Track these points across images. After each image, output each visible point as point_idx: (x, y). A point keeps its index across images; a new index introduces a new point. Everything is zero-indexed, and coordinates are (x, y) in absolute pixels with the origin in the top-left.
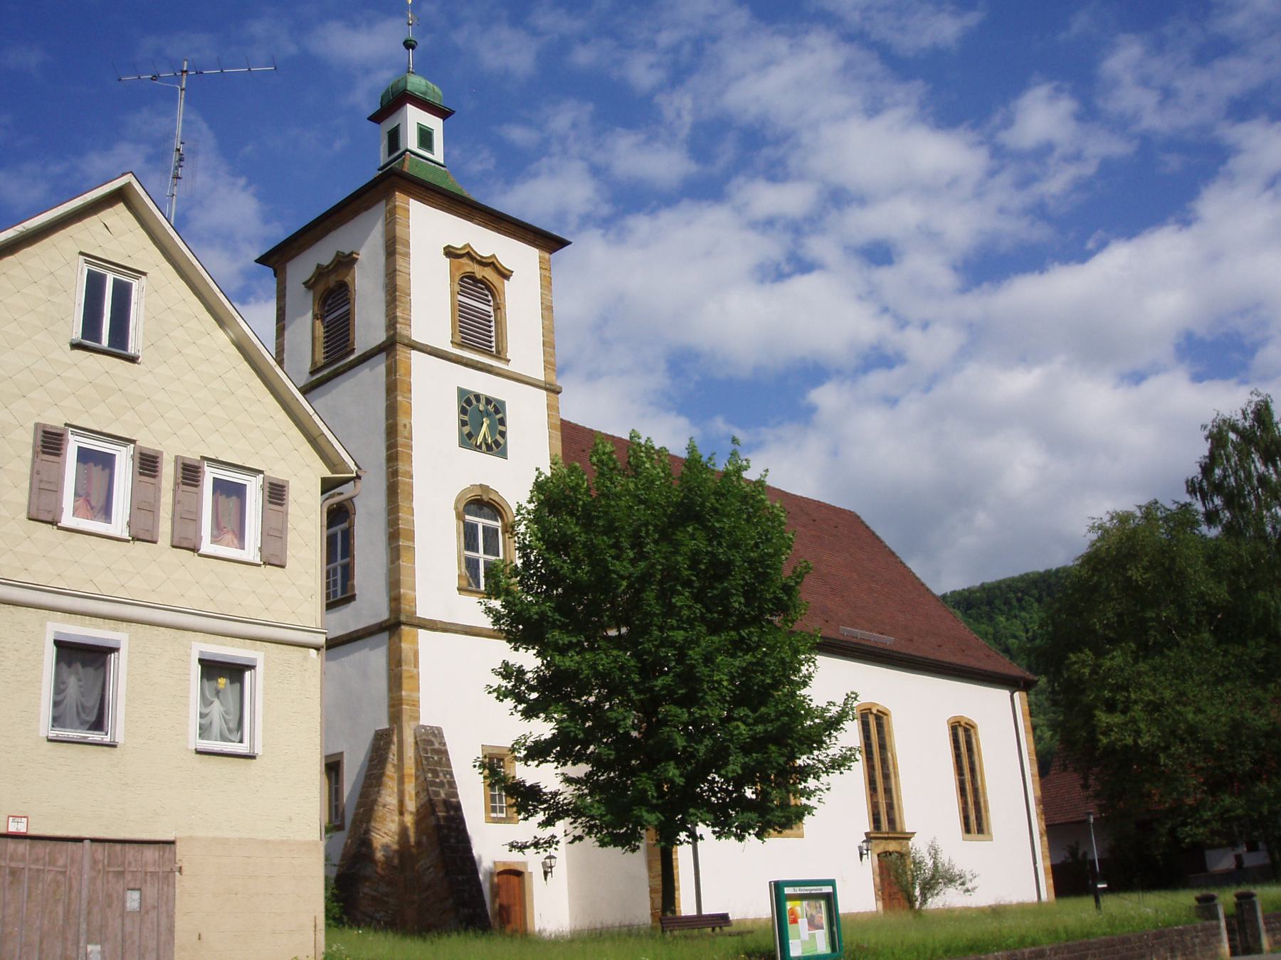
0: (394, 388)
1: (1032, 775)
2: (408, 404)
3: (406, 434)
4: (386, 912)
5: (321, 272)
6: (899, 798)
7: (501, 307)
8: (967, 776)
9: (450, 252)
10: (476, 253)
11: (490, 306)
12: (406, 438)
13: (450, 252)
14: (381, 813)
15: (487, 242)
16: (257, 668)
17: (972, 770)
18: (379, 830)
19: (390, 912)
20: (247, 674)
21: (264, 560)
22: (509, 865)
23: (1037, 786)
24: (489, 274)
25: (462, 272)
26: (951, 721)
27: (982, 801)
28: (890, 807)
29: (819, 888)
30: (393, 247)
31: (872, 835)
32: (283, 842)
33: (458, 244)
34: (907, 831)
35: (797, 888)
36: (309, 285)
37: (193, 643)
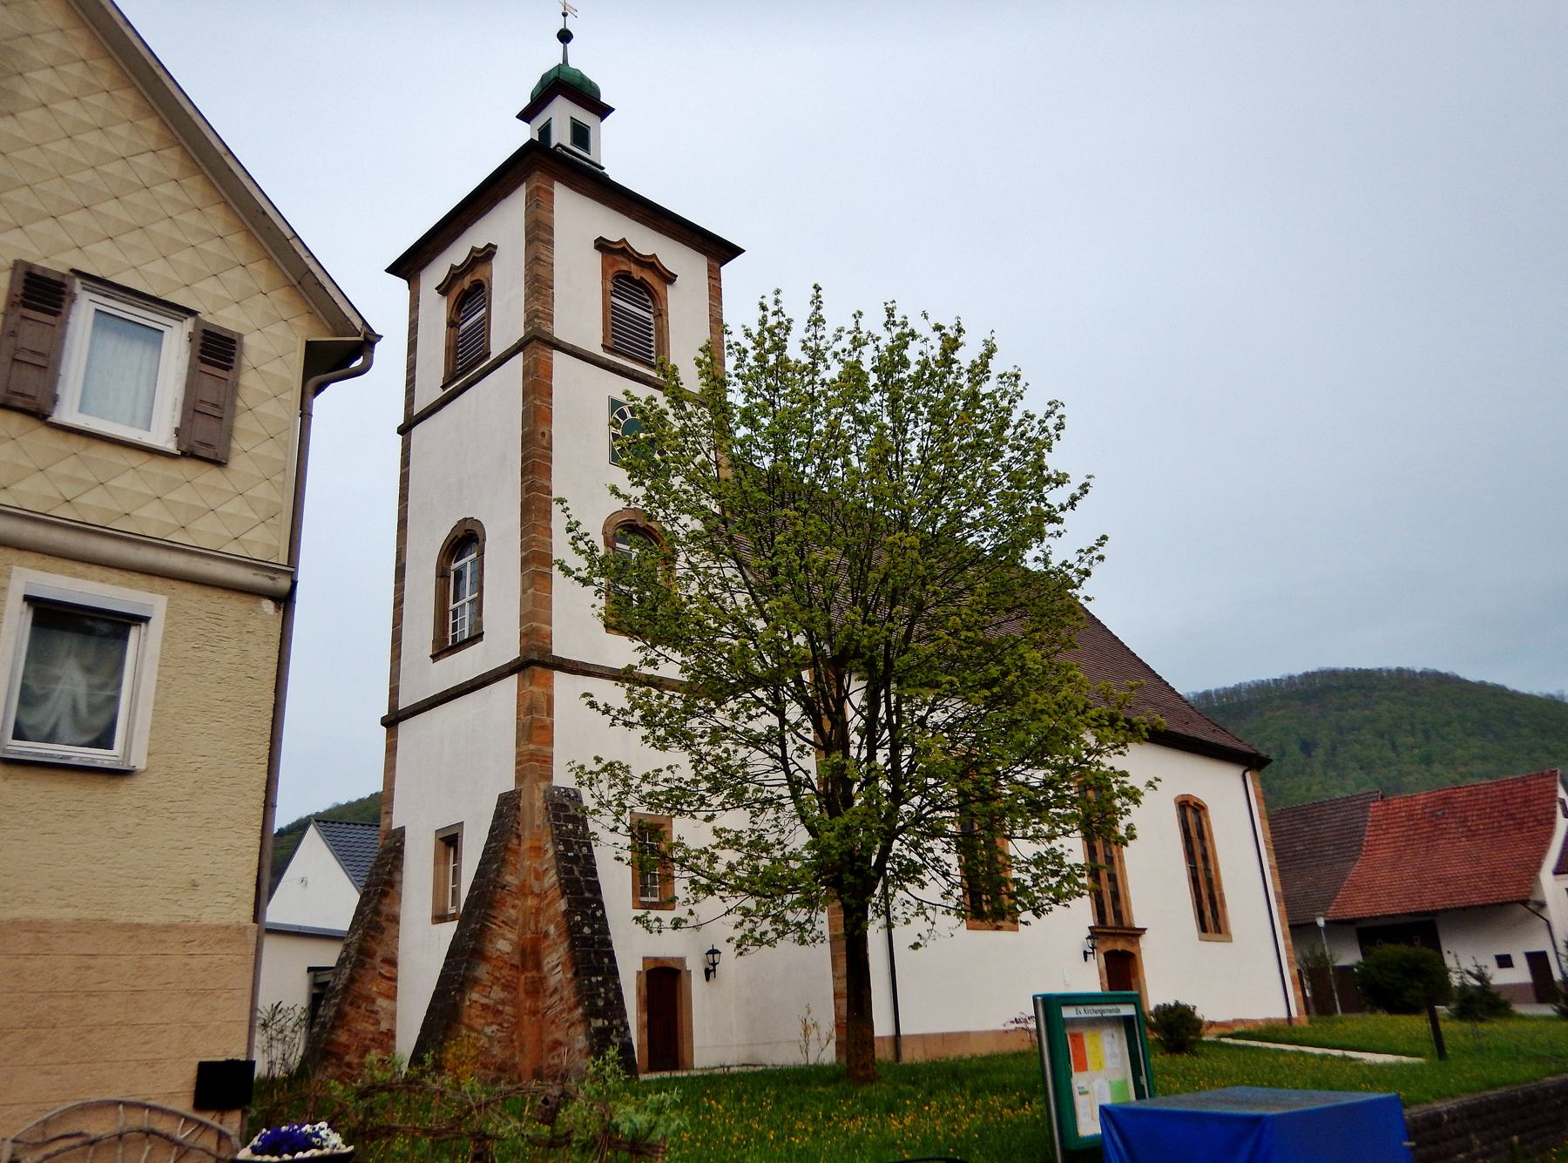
0: (537, 392)
1: (1271, 867)
2: (547, 410)
3: (544, 443)
4: (500, 1025)
5: (456, 274)
6: (1125, 887)
7: (663, 313)
8: (1200, 865)
9: (602, 245)
10: (634, 250)
11: (650, 312)
12: (544, 448)
13: (602, 245)
14: (499, 897)
15: (645, 241)
16: (151, 621)
17: (1205, 858)
18: (494, 917)
19: (506, 1025)
20: (134, 634)
21: (184, 448)
22: (662, 962)
23: (1278, 880)
24: (649, 277)
25: (616, 269)
26: (1179, 800)
27: (1217, 894)
28: (1116, 896)
29: (1113, 1007)
30: (539, 233)
31: (1097, 930)
32: (168, 928)
33: (614, 237)
34: (1137, 926)
35: (1081, 1009)
36: (444, 289)
37: (15, 568)
